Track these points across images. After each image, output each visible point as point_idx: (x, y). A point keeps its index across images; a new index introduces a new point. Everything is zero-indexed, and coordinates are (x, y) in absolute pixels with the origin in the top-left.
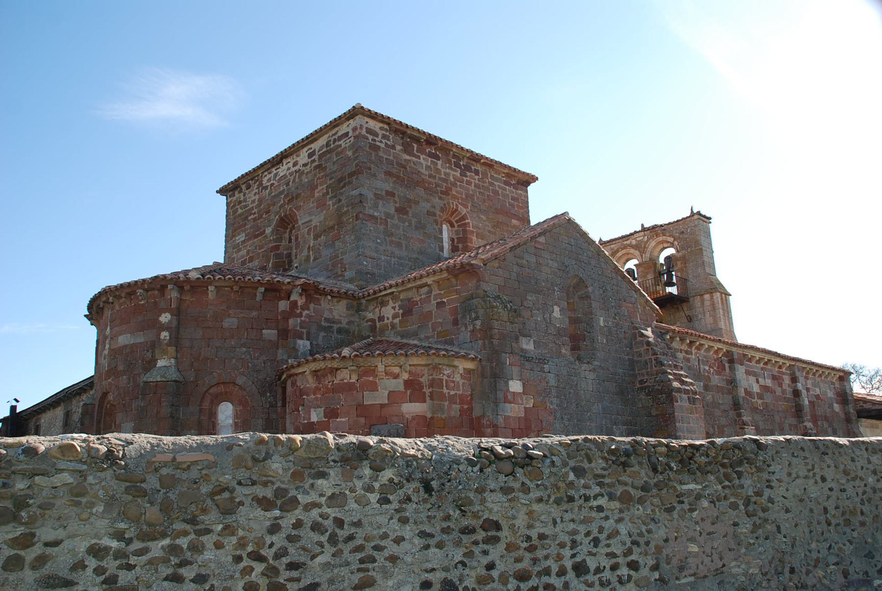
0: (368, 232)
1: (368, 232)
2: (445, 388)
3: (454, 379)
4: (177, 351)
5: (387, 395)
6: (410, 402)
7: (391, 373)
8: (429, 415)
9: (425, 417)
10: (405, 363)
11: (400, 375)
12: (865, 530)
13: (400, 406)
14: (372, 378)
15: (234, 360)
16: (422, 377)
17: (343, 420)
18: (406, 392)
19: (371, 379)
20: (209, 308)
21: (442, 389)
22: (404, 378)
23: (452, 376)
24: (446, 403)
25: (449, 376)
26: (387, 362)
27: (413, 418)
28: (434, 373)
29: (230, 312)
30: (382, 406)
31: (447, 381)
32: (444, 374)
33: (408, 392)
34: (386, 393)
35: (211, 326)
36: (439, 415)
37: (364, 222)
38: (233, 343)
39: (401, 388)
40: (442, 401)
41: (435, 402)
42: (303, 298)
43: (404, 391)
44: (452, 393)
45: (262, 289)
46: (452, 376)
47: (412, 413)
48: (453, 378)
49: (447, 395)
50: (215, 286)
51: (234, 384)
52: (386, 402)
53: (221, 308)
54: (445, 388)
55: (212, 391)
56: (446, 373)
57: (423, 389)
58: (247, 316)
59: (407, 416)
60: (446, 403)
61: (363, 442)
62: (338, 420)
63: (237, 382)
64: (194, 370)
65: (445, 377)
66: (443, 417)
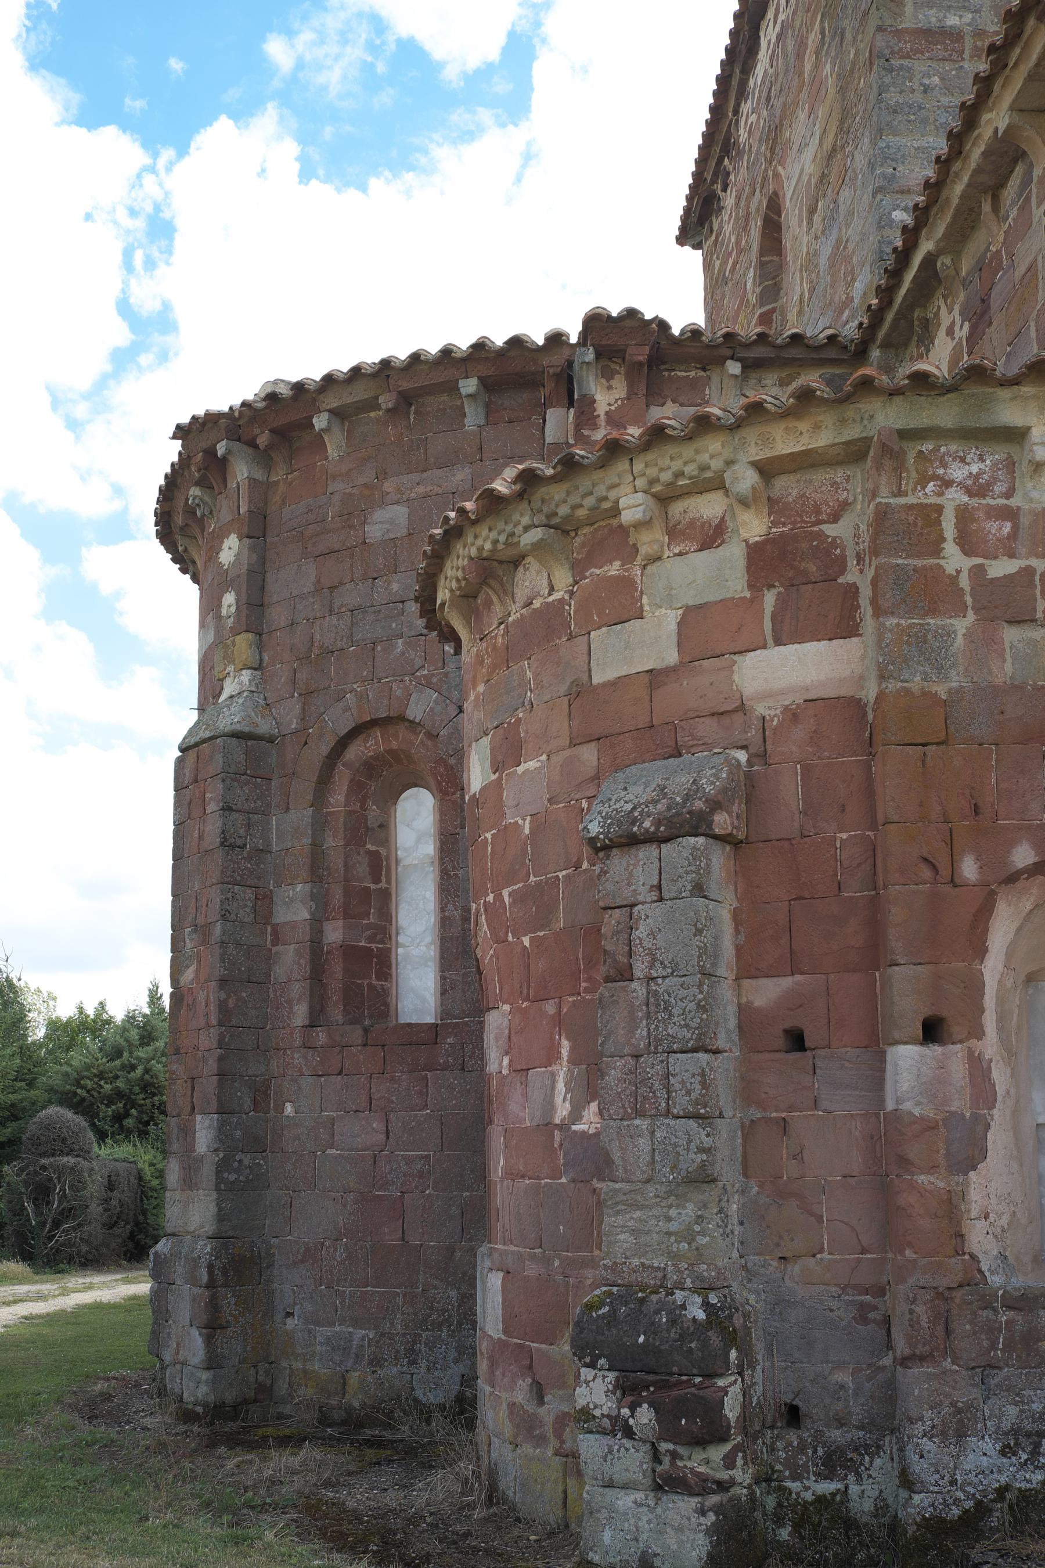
0: (918, 97)
1: (918, 97)
2: (950, 548)
3: (1014, 502)
4: (260, 647)
5: (673, 627)
6: (778, 642)
7: (692, 523)
8: (870, 692)
9: (856, 705)
10: (730, 463)
11: (730, 524)
12: (707, 1462)
13: (730, 668)
14: (617, 564)
15: (400, 641)
16: (835, 518)
17: (532, 765)
18: (756, 600)
19: (614, 569)
20: (330, 489)
21: (936, 550)
22: (744, 535)
23: (999, 488)
24: (962, 625)
25: (977, 489)
26: (652, 472)
27: (792, 715)
28: (884, 480)
29: (388, 486)
30: (655, 677)
31: (964, 515)
32: (948, 483)
33: (770, 599)
34: (671, 618)
35: (336, 547)
36: (916, 683)
37: (896, 62)
38: (395, 586)
39: (737, 585)
40: (933, 612)
41: (891, 621)
42: (614, 383)
43: (748, 594)
44: (1000, 568)
45: (469, 386)
46: (999, 488)
47: (782, 693)
48: (1009, 494)
49: (964, 582)
50: (330, 411)
51: (402, 718)
52: (672, 657)
53: (362, 480)
54: (950, 548)
55: (355, 752)
56: (958, 473)
57: (843, 571)
58: (436, 489)
59: (761, 709)
60: (962, 625)
61: (438, 817)
62: (520, 769)
63: (410, 714)
64: (300, 695)
65: (955, 497)
66: (941, 690)
